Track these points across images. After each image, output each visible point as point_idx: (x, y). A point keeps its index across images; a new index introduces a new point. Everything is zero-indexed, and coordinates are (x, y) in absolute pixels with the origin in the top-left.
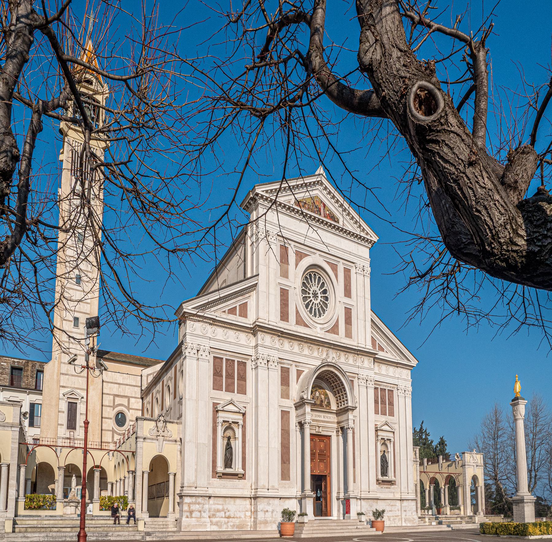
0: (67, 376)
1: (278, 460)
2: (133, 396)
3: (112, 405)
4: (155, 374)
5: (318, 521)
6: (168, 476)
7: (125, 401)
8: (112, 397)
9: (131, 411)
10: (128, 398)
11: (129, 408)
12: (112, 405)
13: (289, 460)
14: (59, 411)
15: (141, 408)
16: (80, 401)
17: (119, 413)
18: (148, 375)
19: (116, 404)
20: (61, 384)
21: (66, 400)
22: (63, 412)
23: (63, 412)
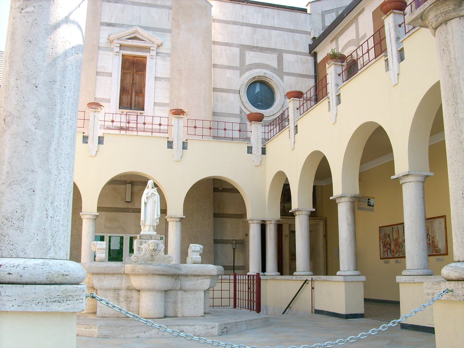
1: (134, 245)
2: (291, 49)
3: (238, 65)
4: (340, 12)
5: (245, 127)
6: (246, 226)
7: (272, 60)
8: (236, 51)
9: (286, 78)
10: (280, 53)
11: (280, 71)
12: (238, 65)
13: (109, 241)
14: (98, 73)
15: (312, 73)
16: (153, 53)
17: (255, 83)
18: (324, 14)
19: (247, 63)
20: (105, 19)
21: (118, 49)
22: (110, 75)
23: (110, 75)
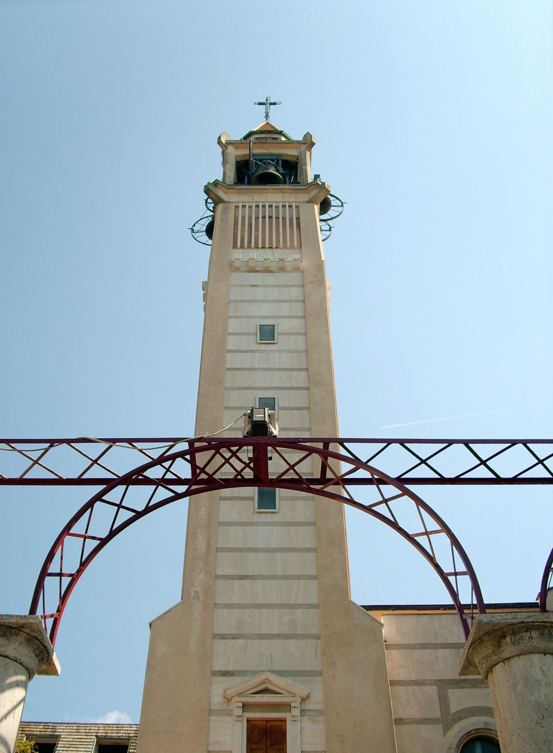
0: (240, 642)
20: (219, 666)
21: (239, 712)
